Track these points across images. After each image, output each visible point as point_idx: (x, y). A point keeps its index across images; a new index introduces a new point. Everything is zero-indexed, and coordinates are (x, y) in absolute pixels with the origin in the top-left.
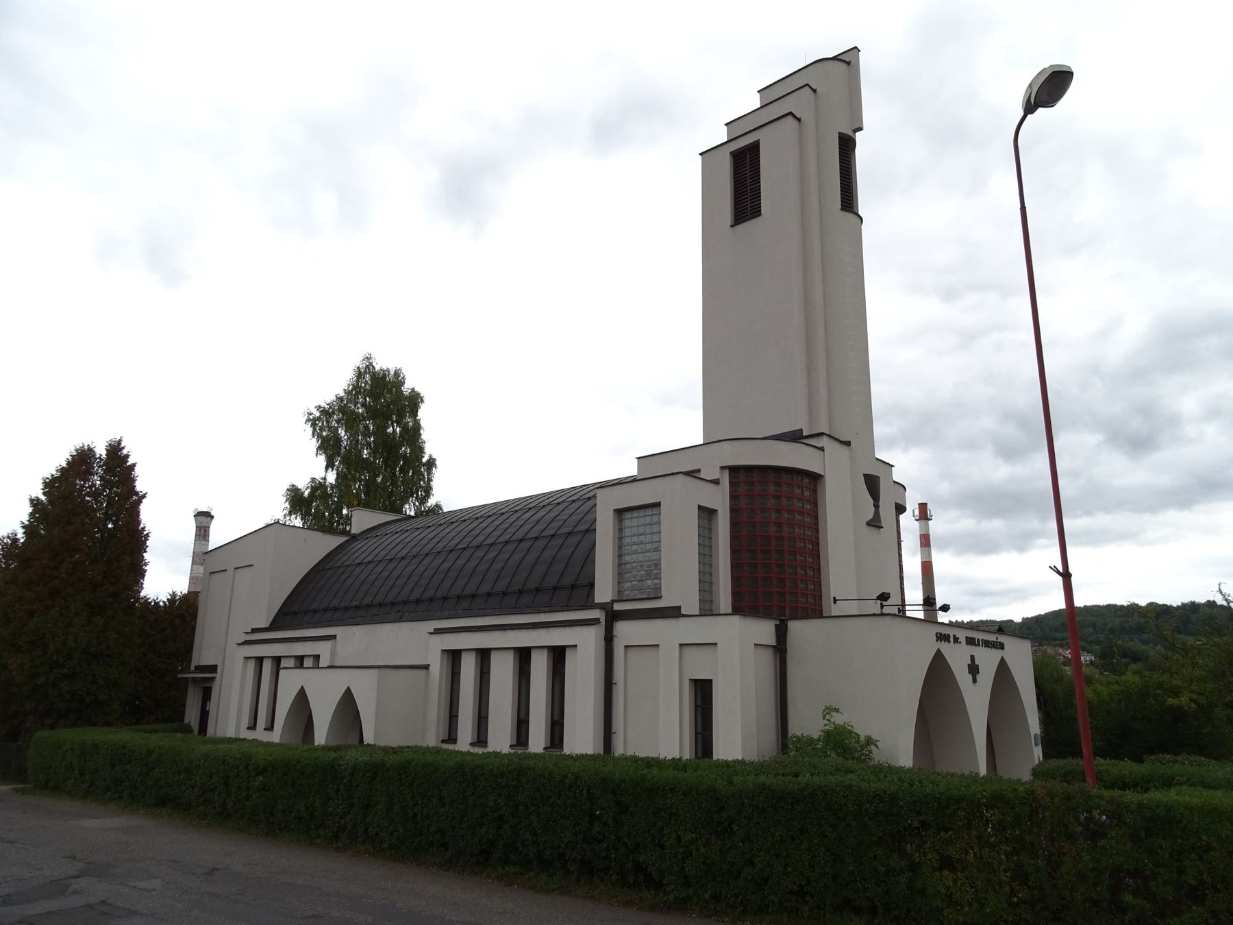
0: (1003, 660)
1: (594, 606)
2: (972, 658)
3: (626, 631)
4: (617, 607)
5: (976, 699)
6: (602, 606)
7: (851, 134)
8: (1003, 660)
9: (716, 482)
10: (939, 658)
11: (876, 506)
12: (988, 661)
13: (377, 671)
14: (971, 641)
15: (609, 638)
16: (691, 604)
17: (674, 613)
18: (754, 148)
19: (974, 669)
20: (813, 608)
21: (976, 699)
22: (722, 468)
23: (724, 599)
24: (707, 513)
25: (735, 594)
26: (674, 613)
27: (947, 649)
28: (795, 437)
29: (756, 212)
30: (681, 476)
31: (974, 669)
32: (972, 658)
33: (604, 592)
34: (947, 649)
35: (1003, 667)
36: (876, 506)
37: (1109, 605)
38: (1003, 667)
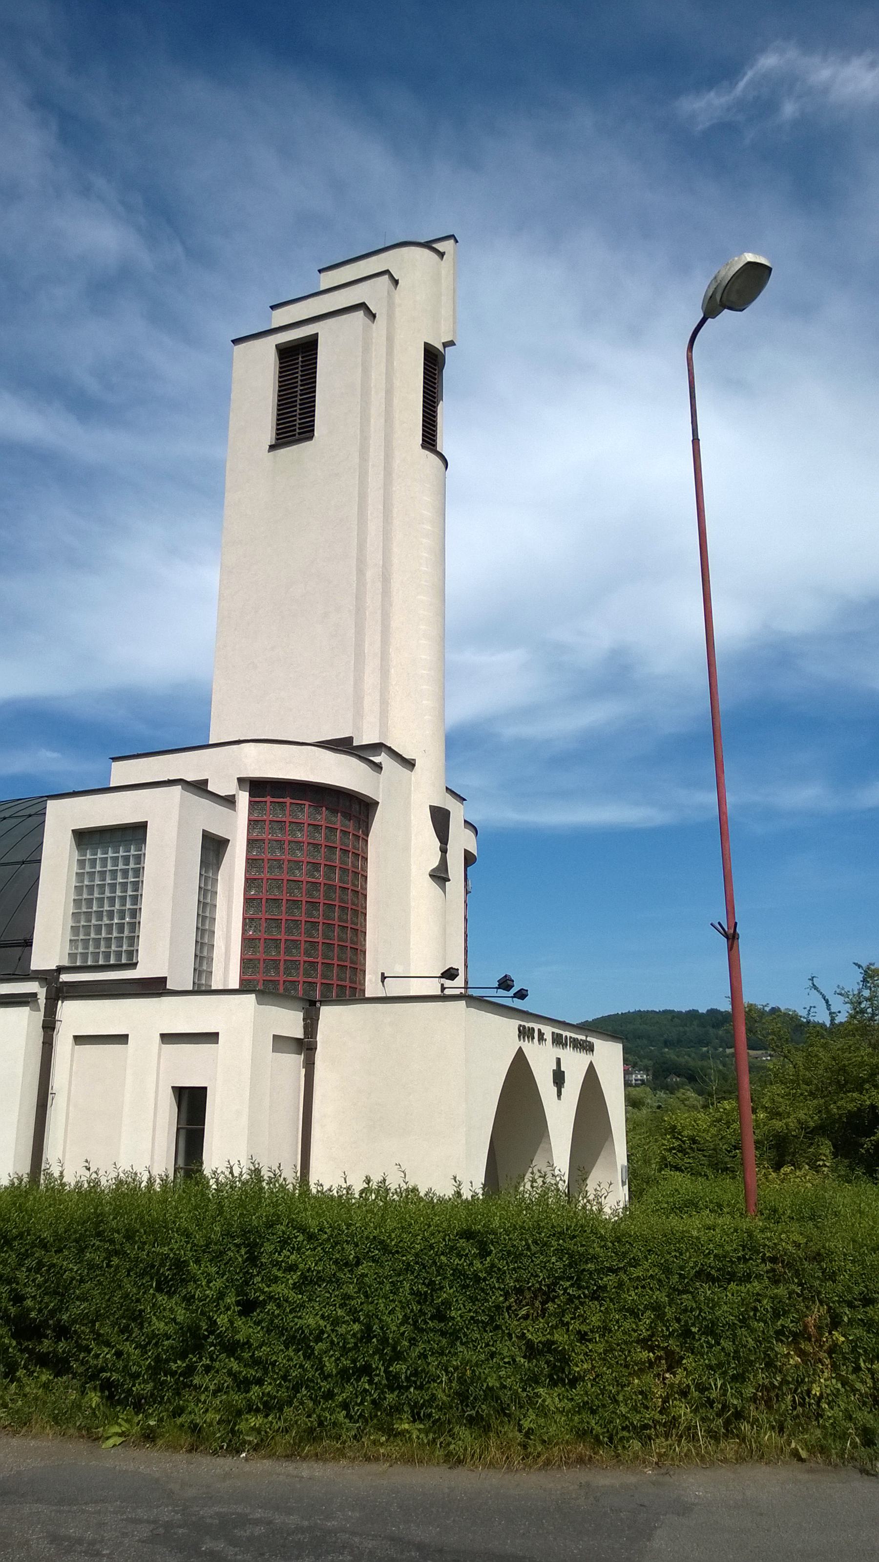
0: (591, 1066)
1: (28, 976)
2: (558, 1061)
3: (76, 1015)
4: (65, 978)
5: (560, 1115)
6: (43, 976)
7: (441, 348)
8: (591, 1066)
9: (229, 801)
10: (520, 1059)
11: (444, 851)
12: (575, 1065)
13: (442, 409)
14: (558, 1040)
15: (49, 1026)
16: (181, 977)
17: (154, 987)
18: (310, 345)
19: (559, 1078)
20: (350, 992)
21: (560, 1115)
22: (240, 780)
23: (227, 968)
24: (214, 847)
25: (246, 964)
26: (154, 987)
27: (531, 1049)
28: (342, 745)
29: (306, 432)
30: (177, 789)
31: (559, 1078)
32: (558, 1061)
33: (49, 948)
34: (531, 1049)
35: (591, 1077)
36: (444, 851)
37: (639, 1014)
38: (591, 1077)
